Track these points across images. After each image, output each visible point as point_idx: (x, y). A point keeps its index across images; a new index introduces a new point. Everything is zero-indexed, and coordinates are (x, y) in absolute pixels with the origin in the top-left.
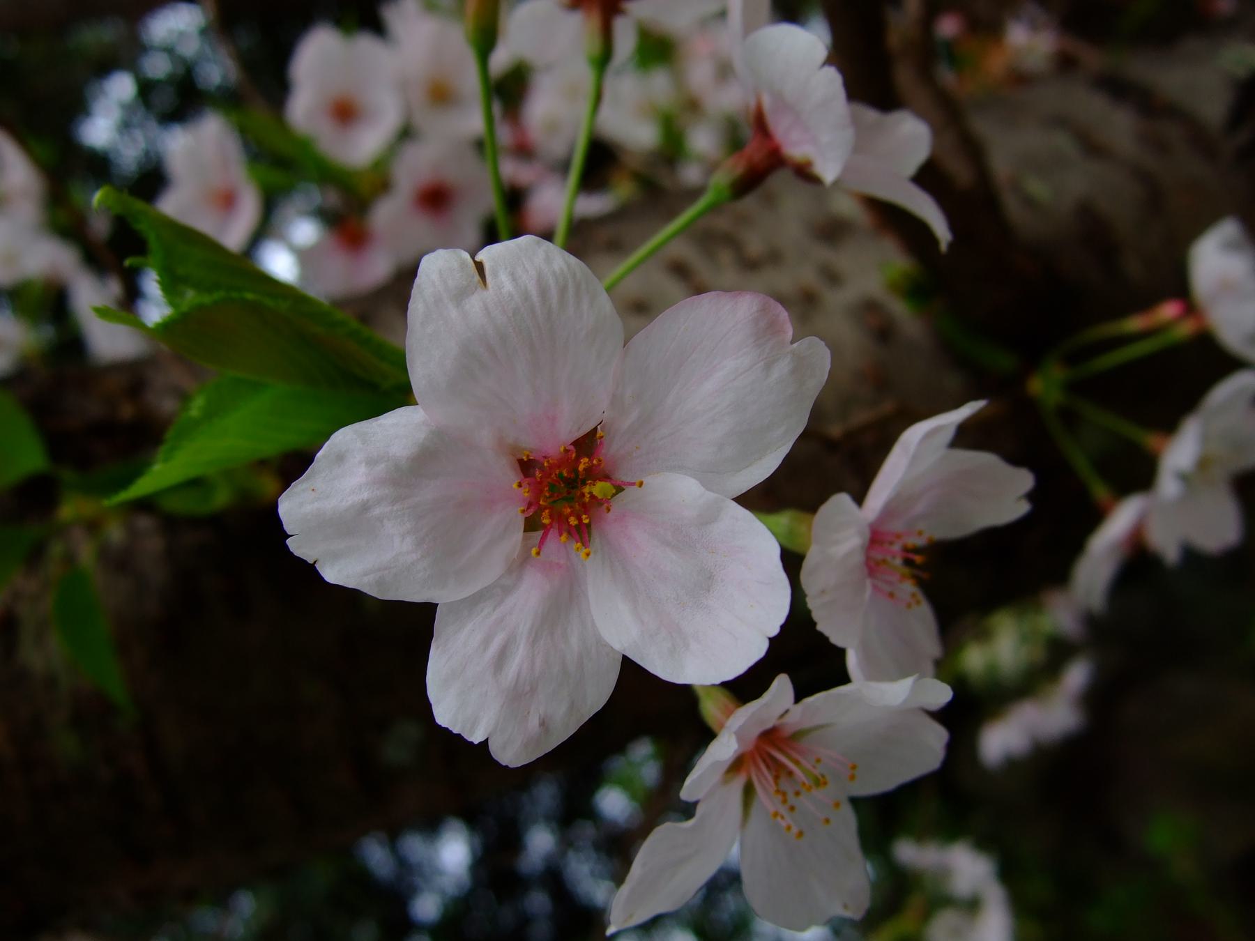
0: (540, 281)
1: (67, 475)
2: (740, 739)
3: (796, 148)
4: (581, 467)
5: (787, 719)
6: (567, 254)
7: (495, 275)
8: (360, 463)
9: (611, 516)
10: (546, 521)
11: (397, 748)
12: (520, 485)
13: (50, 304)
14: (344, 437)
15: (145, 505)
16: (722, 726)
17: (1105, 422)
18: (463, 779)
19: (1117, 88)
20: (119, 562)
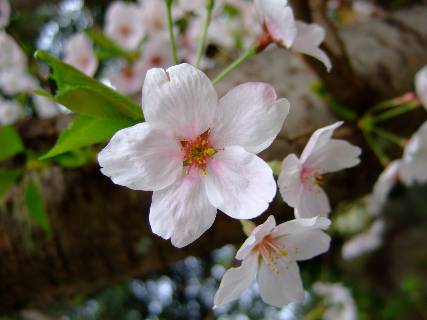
0: (188, 78)
1: (30, 153)
2: (256, 238)
3: (277, 36)
4: (203, 144)
5: (274, 232)
6: (198, 70)
7: (173, 76)
8: (126, 142)
9: (213, 161)
10: (191, 162)
11: (143, 247)
12: (182, 150)
13: (28, 100)
14: (121, 133)
15: (54, 162)
16: (250, 234)
17: (387, 137)
18: (165, 258)
19: (392, 22)
20: (48, 183)
